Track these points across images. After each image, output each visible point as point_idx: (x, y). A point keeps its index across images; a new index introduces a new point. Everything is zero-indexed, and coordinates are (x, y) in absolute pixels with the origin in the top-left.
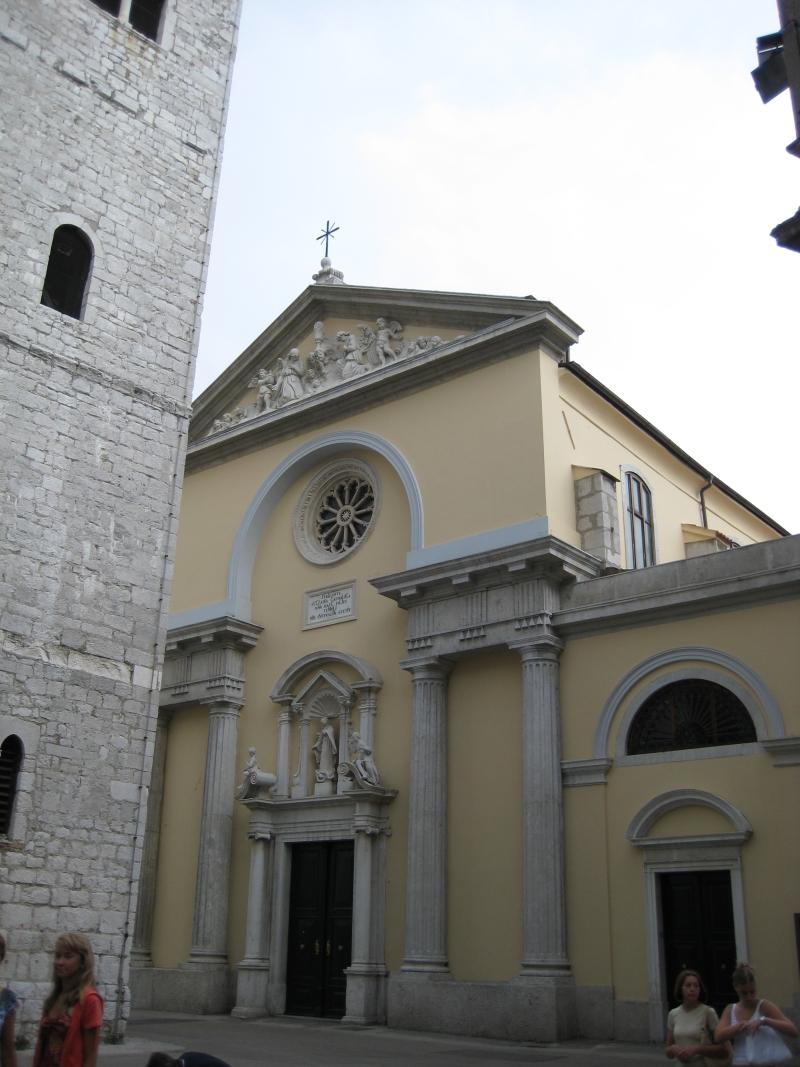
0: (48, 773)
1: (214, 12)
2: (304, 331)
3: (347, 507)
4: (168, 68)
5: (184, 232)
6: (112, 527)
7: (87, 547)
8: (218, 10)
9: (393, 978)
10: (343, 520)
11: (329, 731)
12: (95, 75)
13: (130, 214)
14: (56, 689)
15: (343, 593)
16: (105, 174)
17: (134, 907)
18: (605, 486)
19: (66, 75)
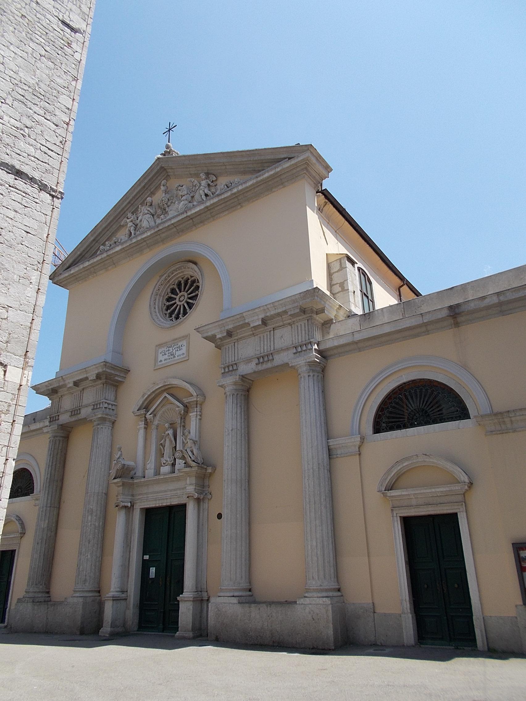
5: (59, 76)
9: (212, 600)
10: (180, 301)
11: (170, 432)
13: (15, 54)
15: (180, 344)
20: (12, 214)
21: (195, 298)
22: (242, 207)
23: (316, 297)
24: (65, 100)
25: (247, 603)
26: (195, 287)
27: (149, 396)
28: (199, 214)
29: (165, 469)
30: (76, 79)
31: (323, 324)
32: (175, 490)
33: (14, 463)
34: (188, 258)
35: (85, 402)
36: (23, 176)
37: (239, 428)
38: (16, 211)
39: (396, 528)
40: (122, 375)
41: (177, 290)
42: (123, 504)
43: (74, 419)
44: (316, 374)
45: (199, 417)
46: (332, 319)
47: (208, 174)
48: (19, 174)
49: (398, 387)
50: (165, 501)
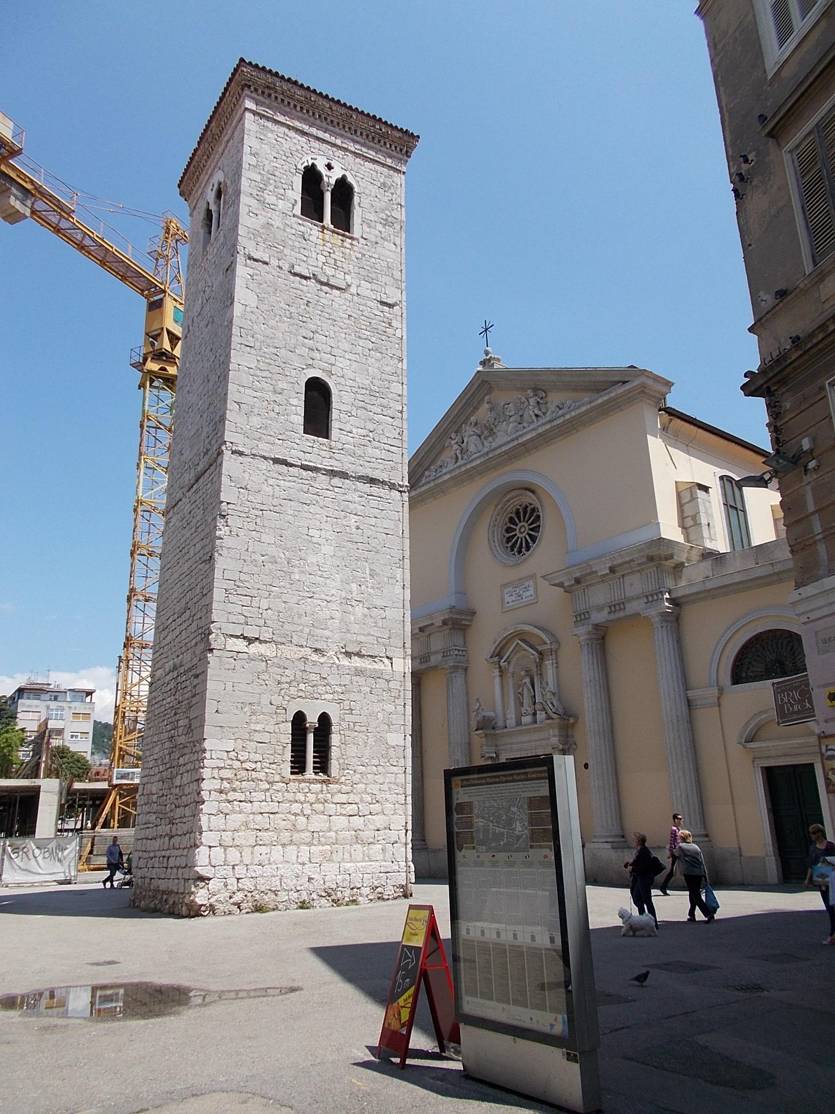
0: (347, 733)
1: (386, 199)
2: (479, 402)
3: (522, 523)
4: (361, 250)
5: (387, 364)
6: (368, 571)
7: (354, 586)
8: (389, 196)
10: (521, 533)
12: (315, 269)
13: (350, 360)
14: (346, 680)
15: (526, 584)
16: (331, 336)
17: (410, 812)
18: (700, 494)
19: (295, 274)
20: (373, 521)
21: (537, 529)
22: (577, 431)
23: (662, 547)
24: (396, 388)
25: (619, 848)
26: (536, 517)
27: (500, 642)
28: (531, 440)
29: (527, 719)
30: (401, 360)
31: (675, 568)
32: (540, 740)
33: (410, 737)
34: (525, 486)
35: (434, 648)
36: (376, 482)
37: (597, 679)
38: (376, 517)
39: (758, 778)
40: (469, 618)
41: (516, 519)
42: (488, 755)
43: (423, 666)
44: (670, 624)
45: (555, 665)
46: (683, 563)
47: (535, 390)
48: (372, 481)
49: (755, 636)
50: (530, 751)
